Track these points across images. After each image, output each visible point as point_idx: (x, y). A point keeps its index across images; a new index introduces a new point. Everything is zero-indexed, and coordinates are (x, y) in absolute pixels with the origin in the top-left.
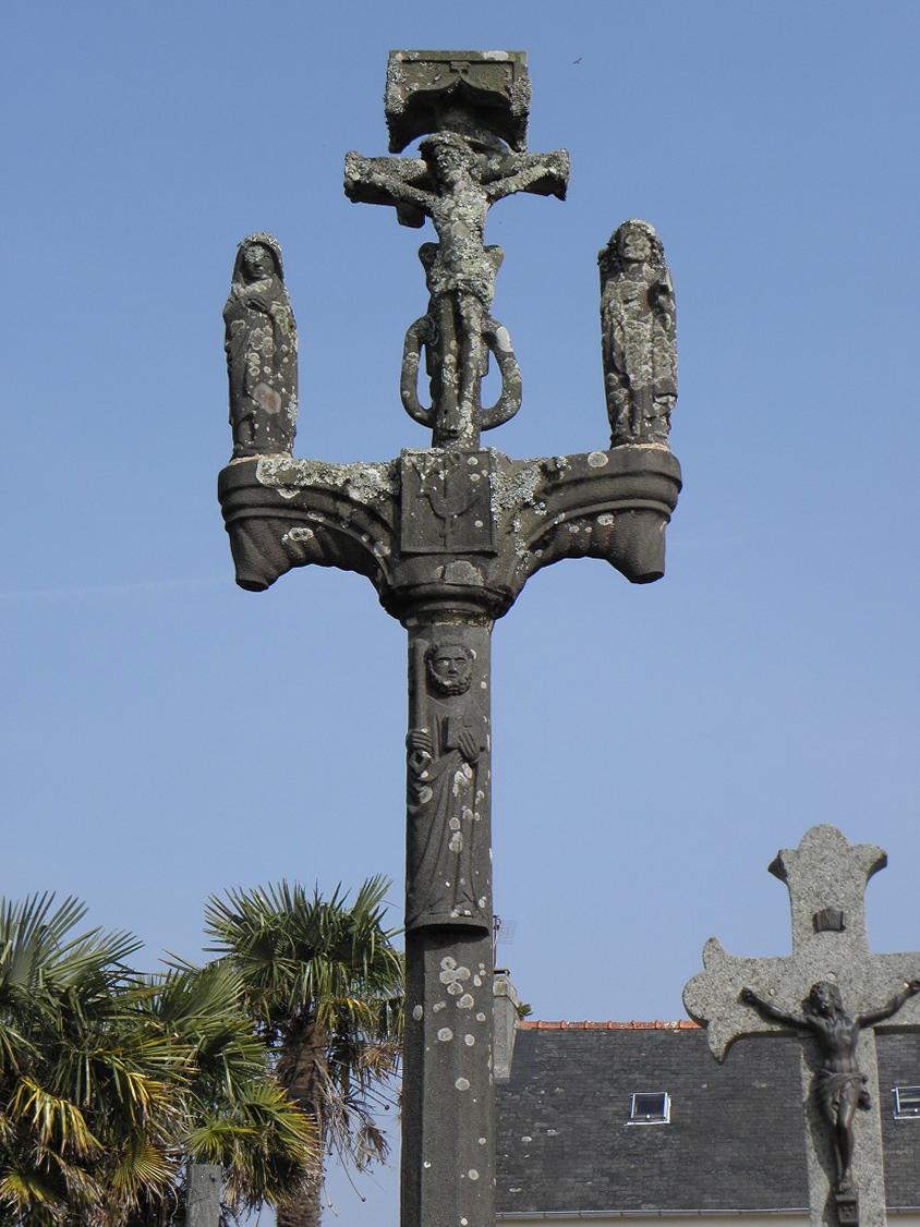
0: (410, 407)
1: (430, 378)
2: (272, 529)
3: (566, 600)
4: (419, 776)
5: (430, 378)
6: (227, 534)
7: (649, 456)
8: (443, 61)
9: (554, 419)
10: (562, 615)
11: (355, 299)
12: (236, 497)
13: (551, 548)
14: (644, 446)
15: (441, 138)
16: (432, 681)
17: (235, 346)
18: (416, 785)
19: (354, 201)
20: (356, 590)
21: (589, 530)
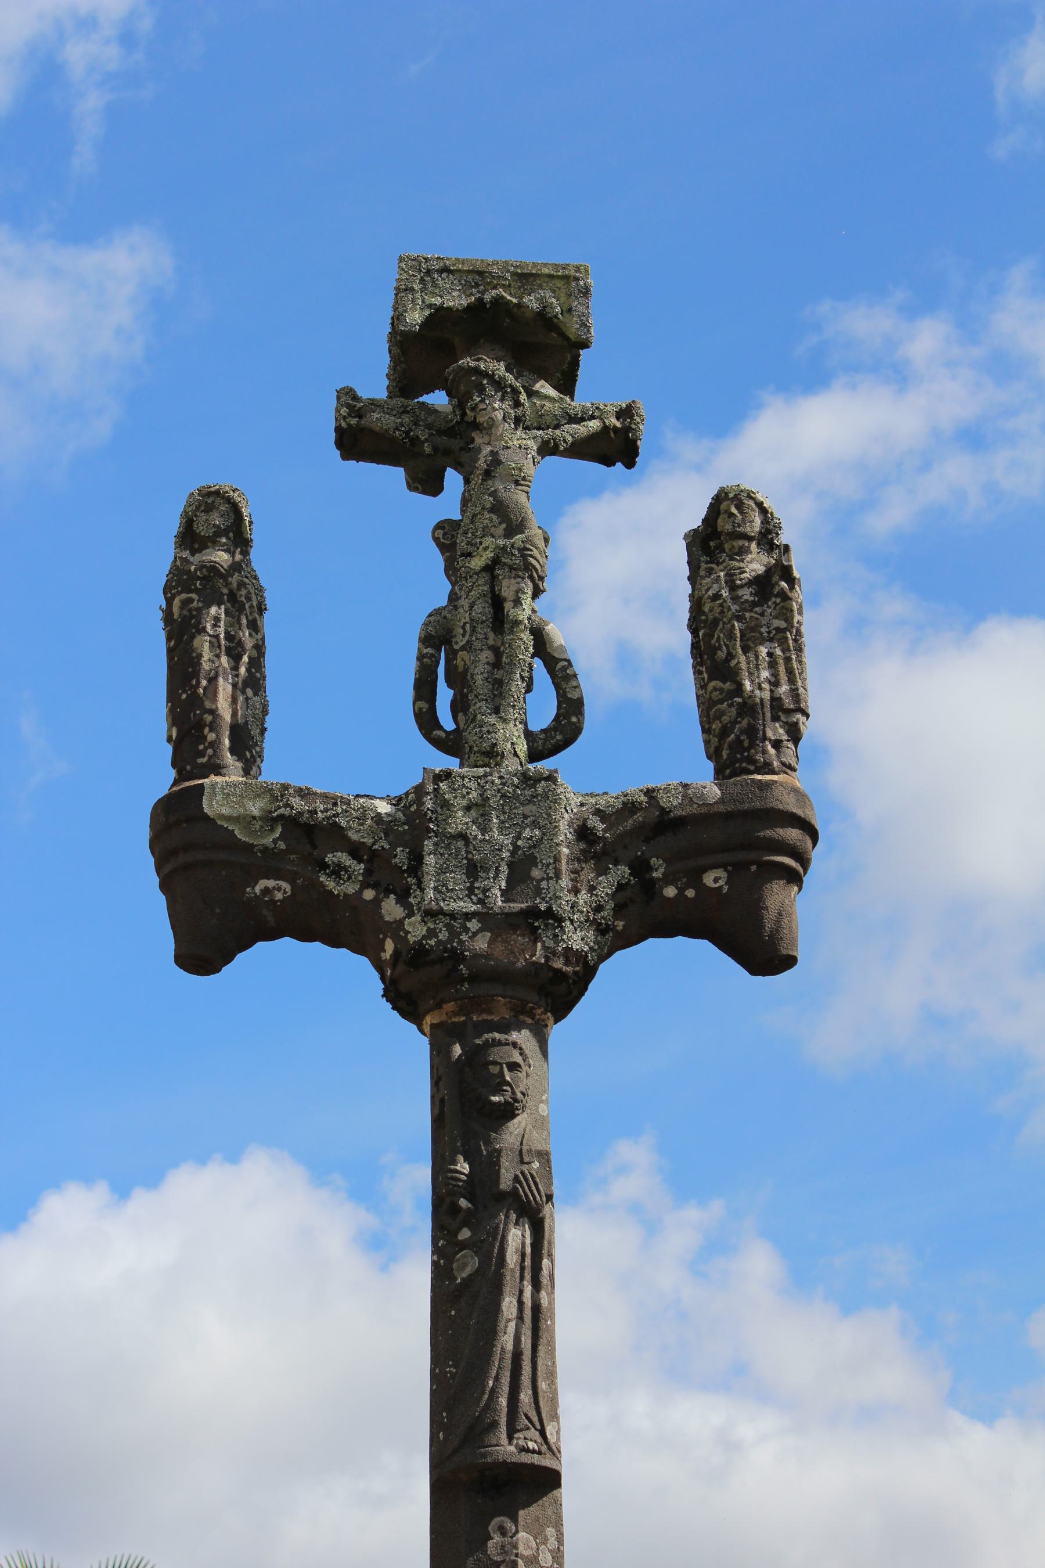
0: (427, 721)
1: (452, 692)
2: (232, 882)
3: (661, 989)
4: (456, 1236)
5: (452, 692)
6: (162, 899)
7: (777, 791)
8: (478, 275)
9: (642, 738)
10: (640, 1031)
11: (352, 576)
12: (180, 832)
13: (641, 916)
14: (769, 777)
15: (472, 364)
16: (470, 1107)
17: (181, 631)
18: (773, 680)
19: (346, 456)
20: (350, 978)
21: (690, 893)
